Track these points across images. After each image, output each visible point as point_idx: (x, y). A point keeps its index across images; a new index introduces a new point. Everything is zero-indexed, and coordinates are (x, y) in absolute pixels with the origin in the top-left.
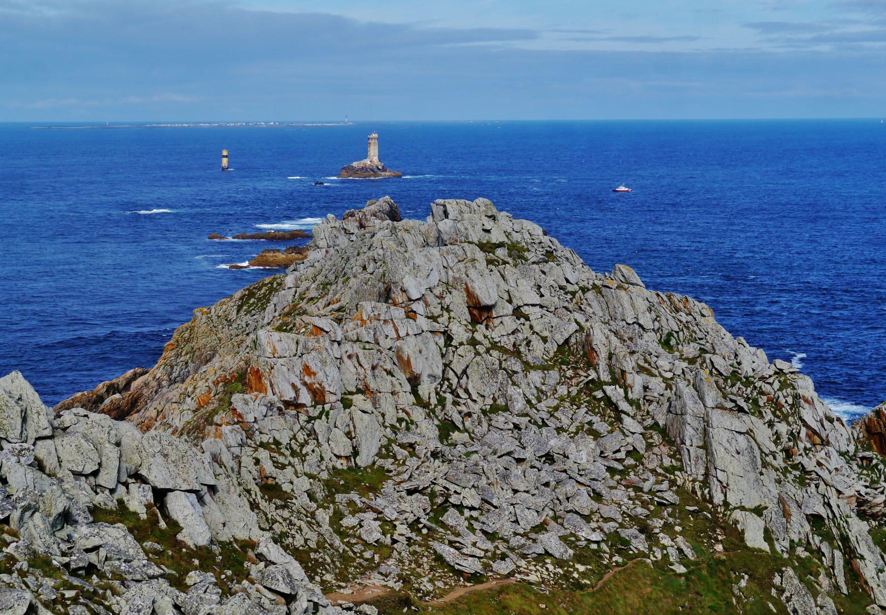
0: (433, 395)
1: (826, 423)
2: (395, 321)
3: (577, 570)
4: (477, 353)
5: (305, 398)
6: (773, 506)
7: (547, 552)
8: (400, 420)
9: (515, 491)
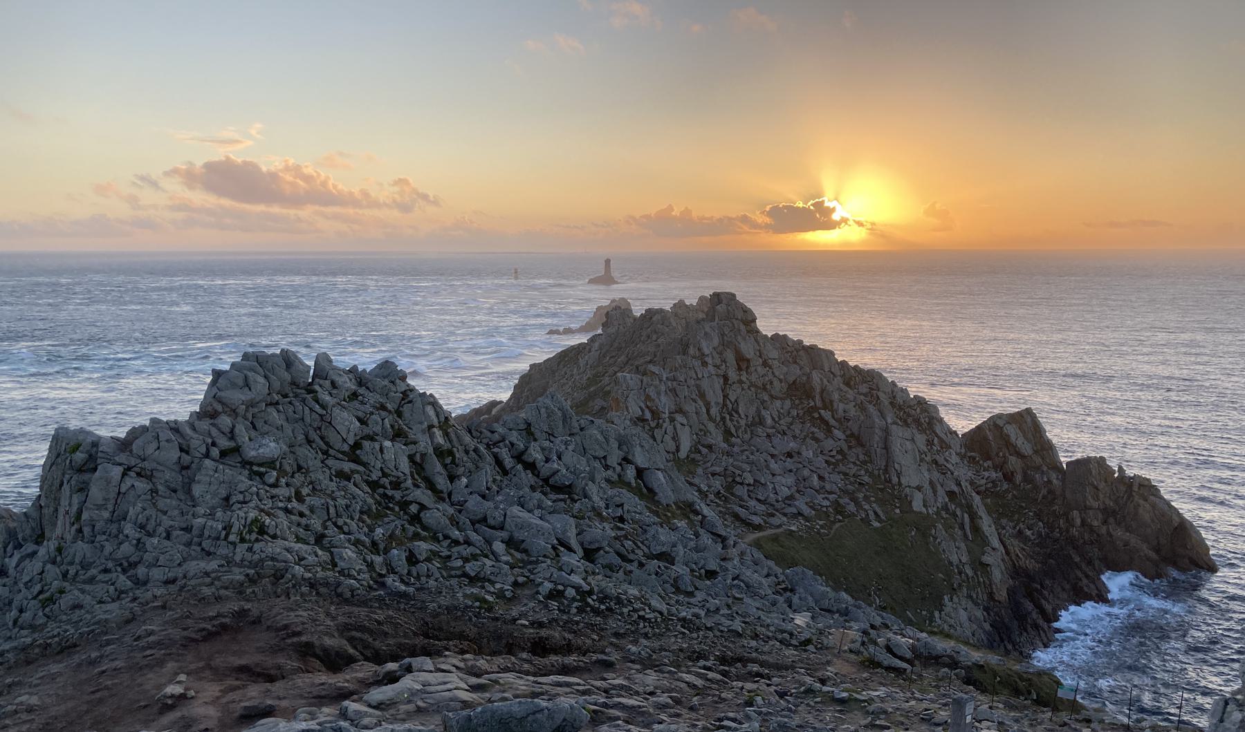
0: (718, 414)
3: (818, 524)
4: (743, 389)
5: (648, 415)
6: (926, 485)
7: (799, 513)
8: (701, 430)
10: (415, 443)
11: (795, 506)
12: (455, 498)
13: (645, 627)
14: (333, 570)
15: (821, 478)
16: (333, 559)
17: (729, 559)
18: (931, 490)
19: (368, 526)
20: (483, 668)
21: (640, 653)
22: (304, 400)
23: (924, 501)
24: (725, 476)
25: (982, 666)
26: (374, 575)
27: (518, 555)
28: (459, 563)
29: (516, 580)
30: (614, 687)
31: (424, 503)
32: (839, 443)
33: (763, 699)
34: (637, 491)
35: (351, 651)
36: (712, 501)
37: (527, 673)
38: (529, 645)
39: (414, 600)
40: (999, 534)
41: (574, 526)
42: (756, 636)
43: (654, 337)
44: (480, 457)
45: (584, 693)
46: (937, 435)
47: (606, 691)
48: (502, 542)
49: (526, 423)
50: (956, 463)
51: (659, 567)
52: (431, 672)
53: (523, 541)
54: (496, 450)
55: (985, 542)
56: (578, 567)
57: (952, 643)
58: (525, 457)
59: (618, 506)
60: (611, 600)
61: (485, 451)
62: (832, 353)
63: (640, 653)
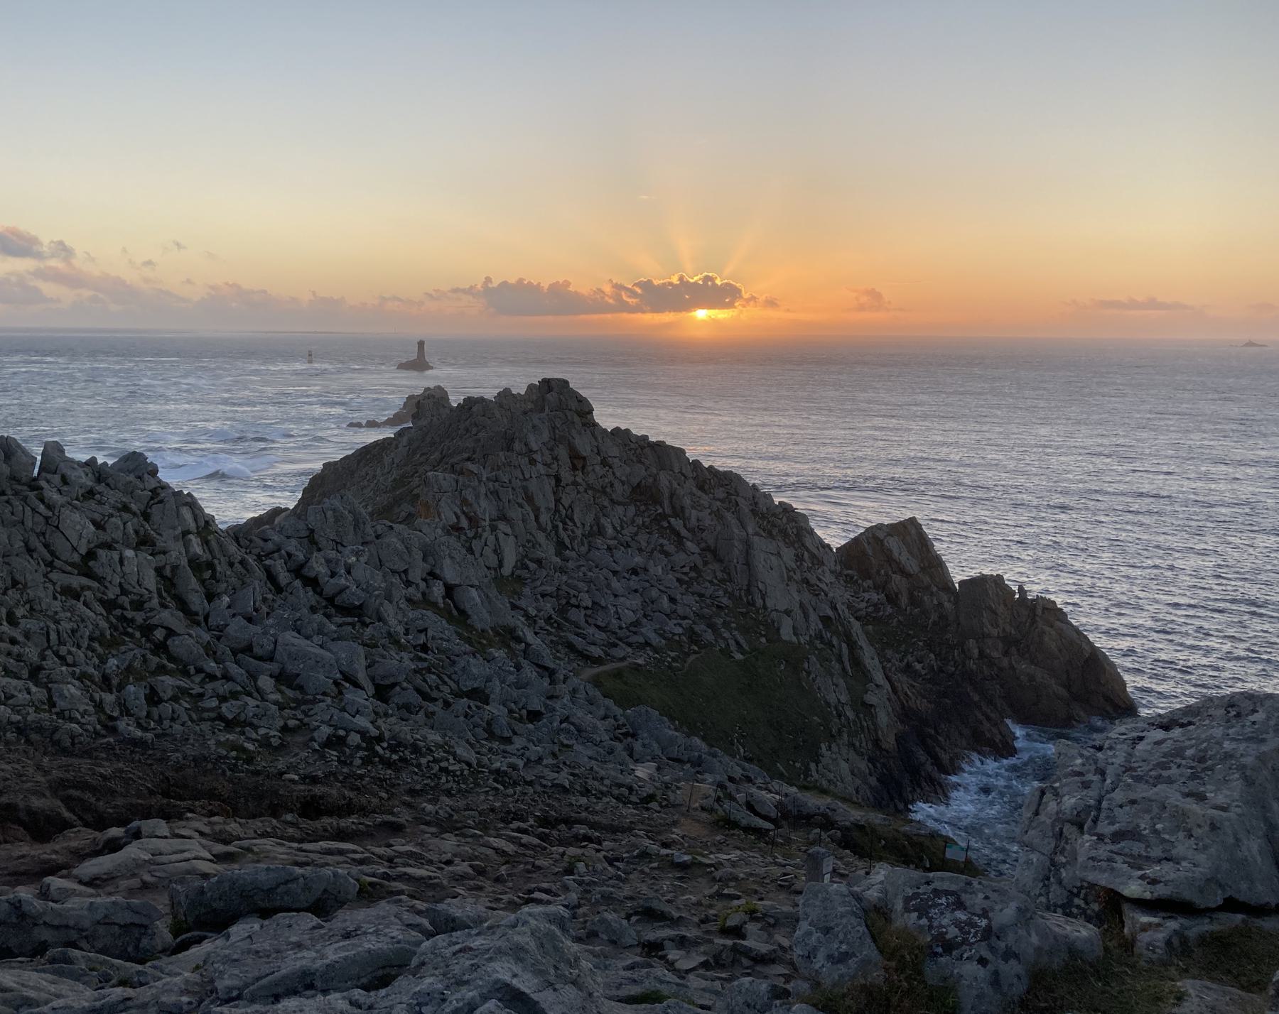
0: (549, 522)
5: (464, 523)
6: (797, 611)
8: (528, 541)
10: (164, 553)
11: (642, 634)
13: (448, 781)
14: (50, 711)
15: (672, 600)
16: (50, 698)
17: (557, 697)
19: (99, 656)
20: (235, 833)
21: (437, 813)
22: (25, 499)
25: (863, 827)
26: (103, 717)
27: (290, 693)
28: (214, 703)
30: (401, 854)
32: (692, 558)
33: (587, 866)
35: (67, 814)
36: (541, 628)
37: (292, 839)
38: (298, 805)
39: (153, 749)
40: (884, 668)
41: (363, 656)
42: (586, 792)
43: (474, 430)
44: (247, 570)
45: (361, 862)
46: (808, 550)
47: (390, 860)
48: (271, 676)
49: (308, 529)
51: (469, 707)
52: (166, 837)
53: (298, 675)
54: (268, 562)
55: (866, 677)
56: (366, 707)
57: (829, 800)
58: (305, 571)
59: (420, 631)
60: (406, 748)
61: (254, 564)
62: (683, 451)
63: (437, 813)
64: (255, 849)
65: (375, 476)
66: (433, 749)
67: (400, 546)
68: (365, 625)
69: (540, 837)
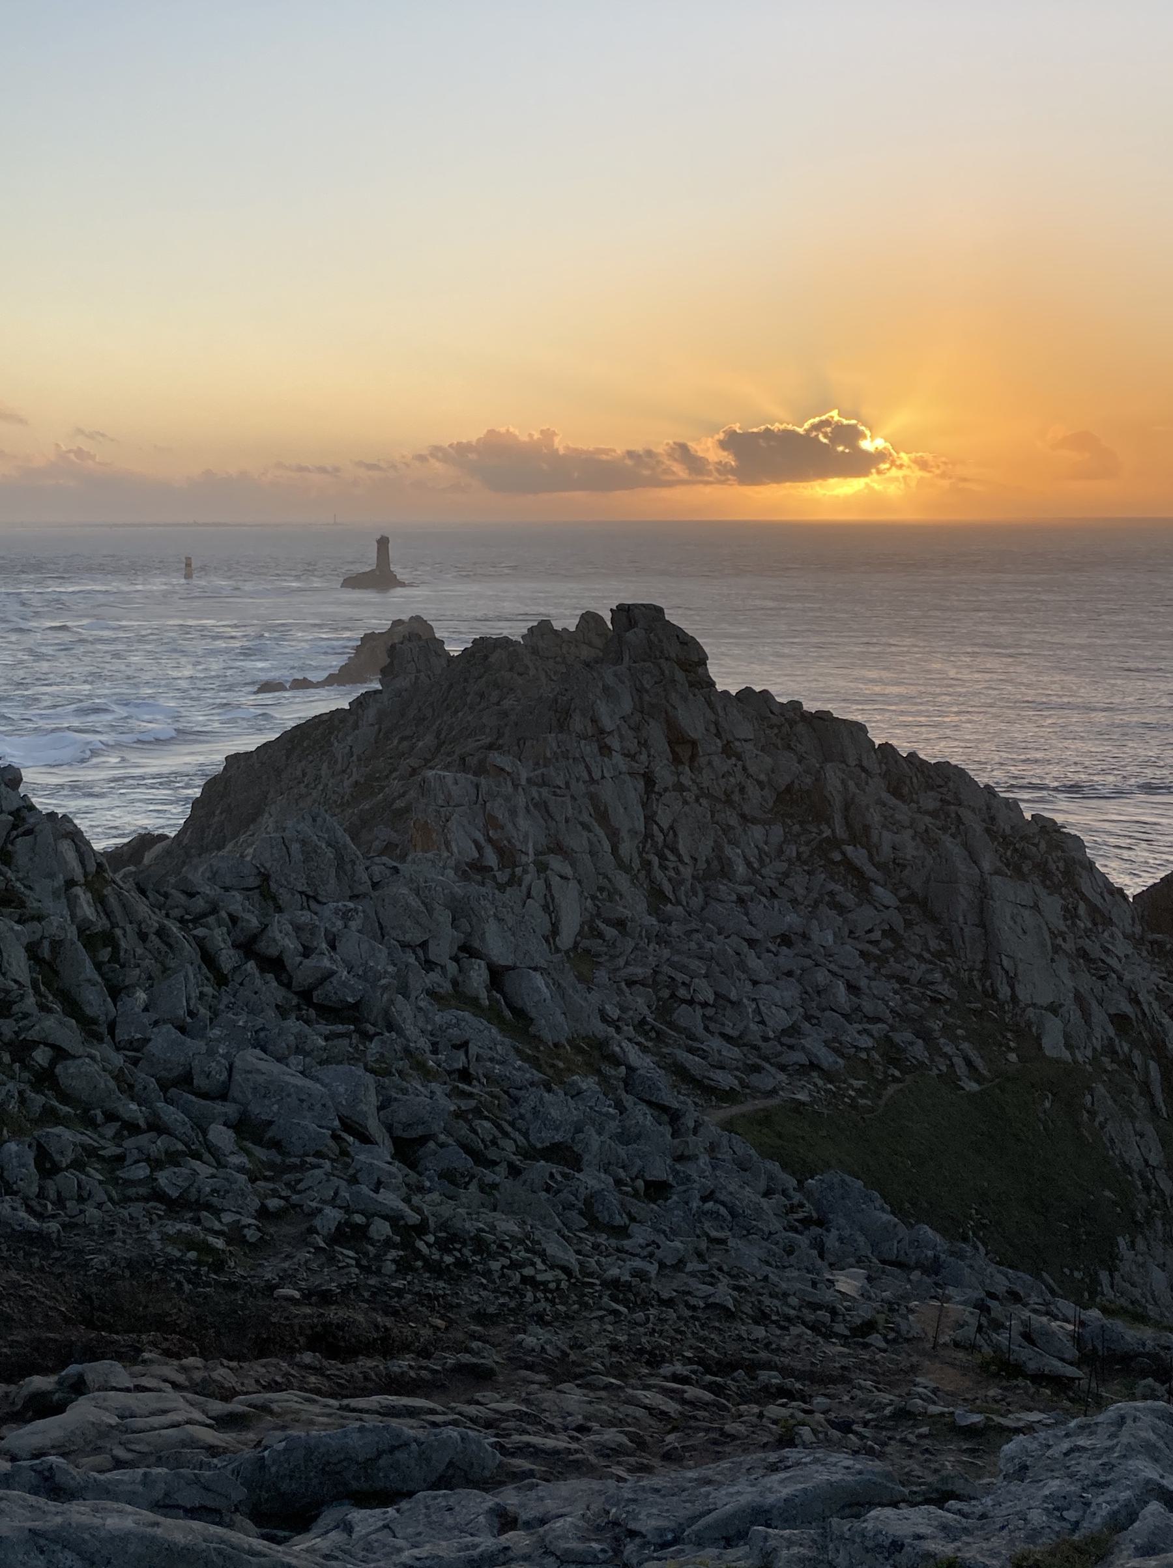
0: (636, 855)
1: (1107, 897)
2: (587, 759)
3: (851, 1086)
4: (686, 802)
5: (491, 859)
7: (811, 1063)
8: (601, 889)
9: (755, 983)
10: (39, 918)
12: (122, 1034)
13: (537, 1300)
15: (853, 988)
18: (1079, 1013)
21: (543, 1347)
23: (1067, 1036)
24: (655, 985)
27: (261, 1153)
28: (141, 1171)
29: (263, 1206)
31: (63, 1046)
34: (492, 1015)
39: (60, 1249)
42: (762, 1317)
46: (1083, 897)
50: (1127, 956)
51: (552, 1176)
53: (271, 1123)
54: (200, 932)
56: (391, 1175)
60: (464, 1244)
64: (274, 1406)
65: (318, 778)
66: (508, 1245)
67: (414, 902)
68: (367, 1037)
69: (709, 1387)
